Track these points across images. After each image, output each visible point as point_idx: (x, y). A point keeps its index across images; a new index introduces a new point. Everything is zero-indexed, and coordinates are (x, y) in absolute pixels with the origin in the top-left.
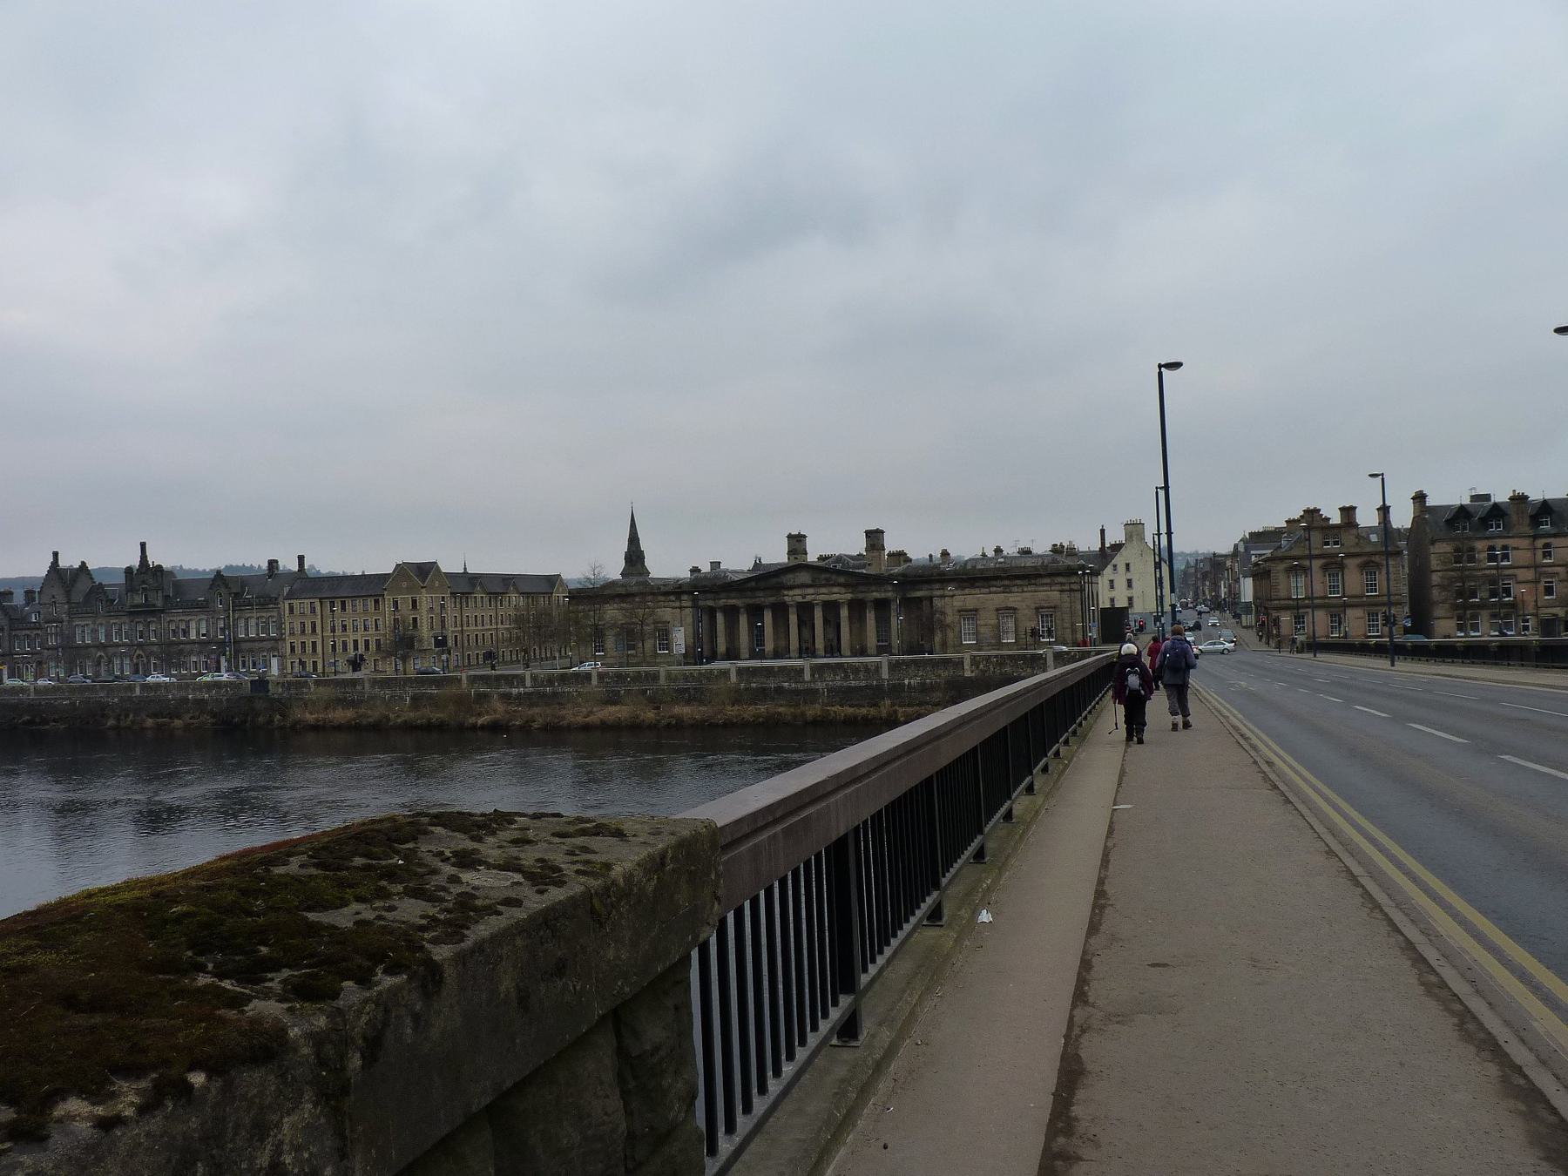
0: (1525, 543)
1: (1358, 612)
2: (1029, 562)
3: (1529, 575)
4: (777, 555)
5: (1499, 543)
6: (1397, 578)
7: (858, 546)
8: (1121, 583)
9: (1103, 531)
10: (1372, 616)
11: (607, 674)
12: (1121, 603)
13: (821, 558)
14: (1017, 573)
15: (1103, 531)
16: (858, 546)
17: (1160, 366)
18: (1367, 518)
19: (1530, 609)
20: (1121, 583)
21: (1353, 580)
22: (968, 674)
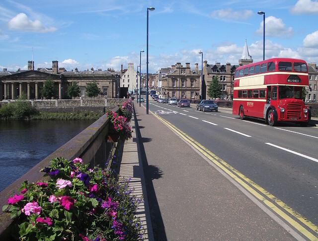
0: (229, 76)
1: (189, 92)
2: (101, 73)
3: (229, 84)
4: (25, 68)
5: (223, 76)
6: (198, 83)
7: (50, 65)
8: (126, 80)
9: (122, 65)
10: (192, 93)
11: (279, 97)
12: (126, 86)
13: (39, 69)
14: (86, 147)
15: (122, 65)
16: (50, 65)
17: (148, 9)
18: (193, 67)
19: (229, 93)
20: (126, 80)
21: (188, 83)
22: (81, 105)
